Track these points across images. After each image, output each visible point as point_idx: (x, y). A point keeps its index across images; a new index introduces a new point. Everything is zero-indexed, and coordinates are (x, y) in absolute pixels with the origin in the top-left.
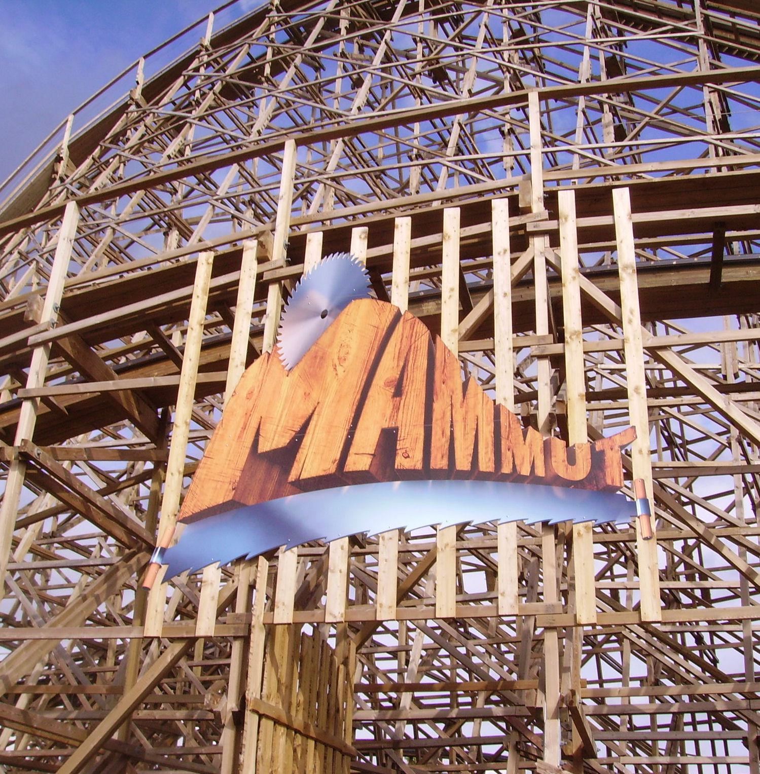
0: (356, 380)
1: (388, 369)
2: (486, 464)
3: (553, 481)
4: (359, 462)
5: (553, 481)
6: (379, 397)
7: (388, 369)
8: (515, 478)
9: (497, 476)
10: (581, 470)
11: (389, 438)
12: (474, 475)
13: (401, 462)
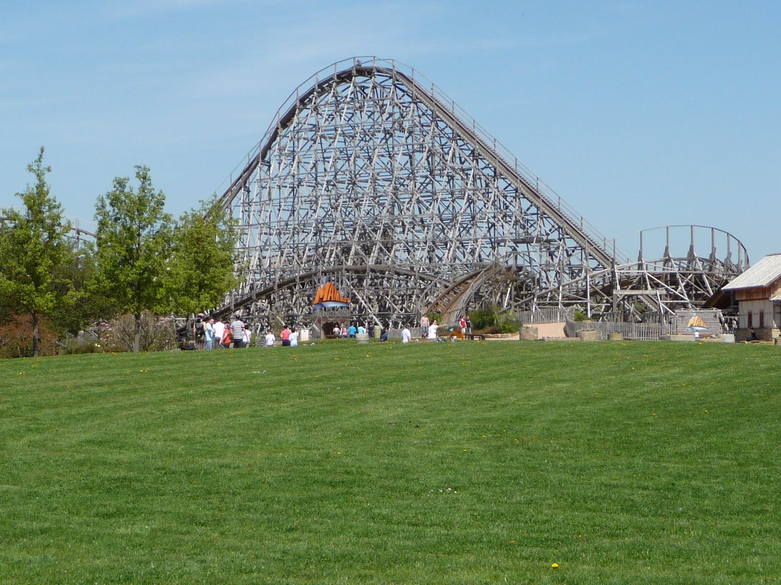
4: (328, 300)
11: (331, 297)
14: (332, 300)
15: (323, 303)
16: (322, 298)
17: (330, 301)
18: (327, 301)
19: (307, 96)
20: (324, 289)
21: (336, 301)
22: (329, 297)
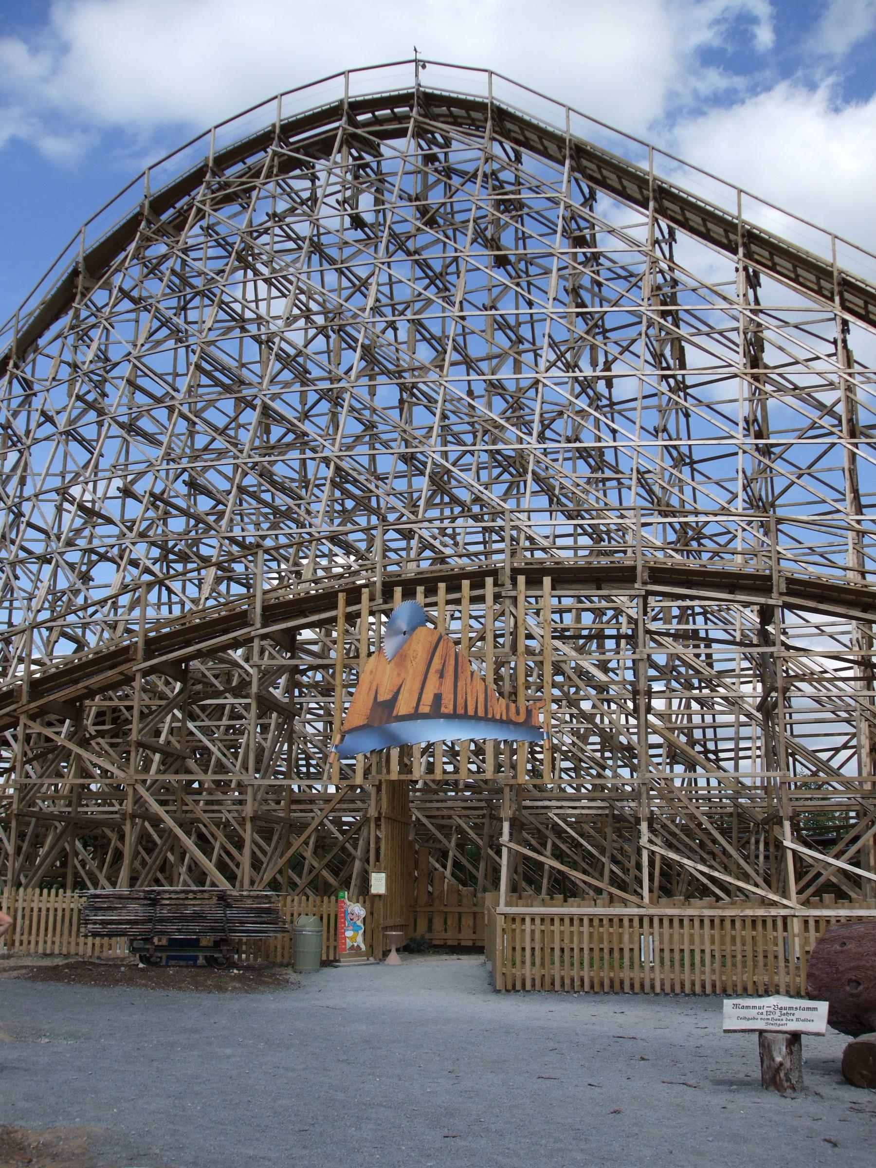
0: (422, 668)
1: (436, 664)
2: (481, 713)
4: (425, 709)
6: (433, 679)
7: (436, 664)
10: (522, 718)
11: (438, 698)
13: (443, 710)
16: (391, 703)
17: (436, 713)
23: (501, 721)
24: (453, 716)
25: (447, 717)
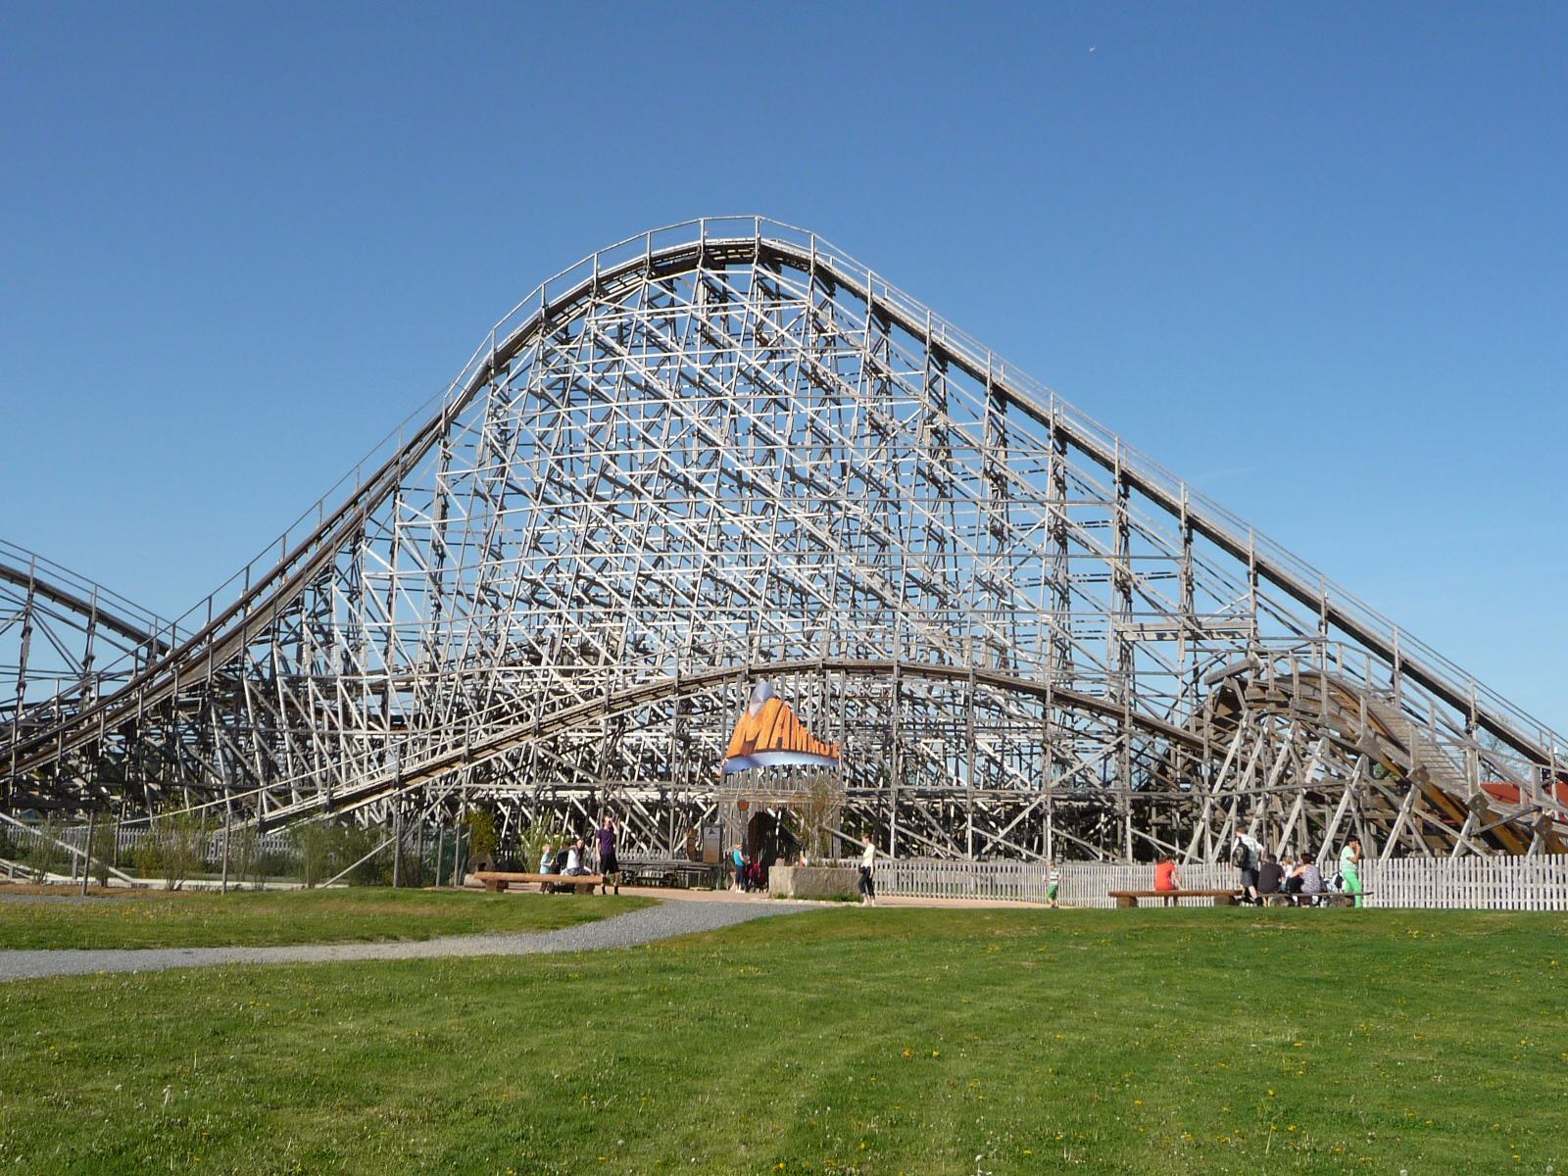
2: (804, 749)
3: (820, 755)
4: (773, 746)
5: (820, 755)
6: (777, 727)
8: (811, 753)
9: (807, 752)
12: (801, 752)
14: (785, 746)
15: (755, 755)
16: (754, 742)
17: (779, 748)
18: (767, 750)
19: (560, 308)
20: (759, 715)
21: (795, 751)
22: (774, 740)
23: (815, 754)
24: (789, 751)
25: (785, 751)
